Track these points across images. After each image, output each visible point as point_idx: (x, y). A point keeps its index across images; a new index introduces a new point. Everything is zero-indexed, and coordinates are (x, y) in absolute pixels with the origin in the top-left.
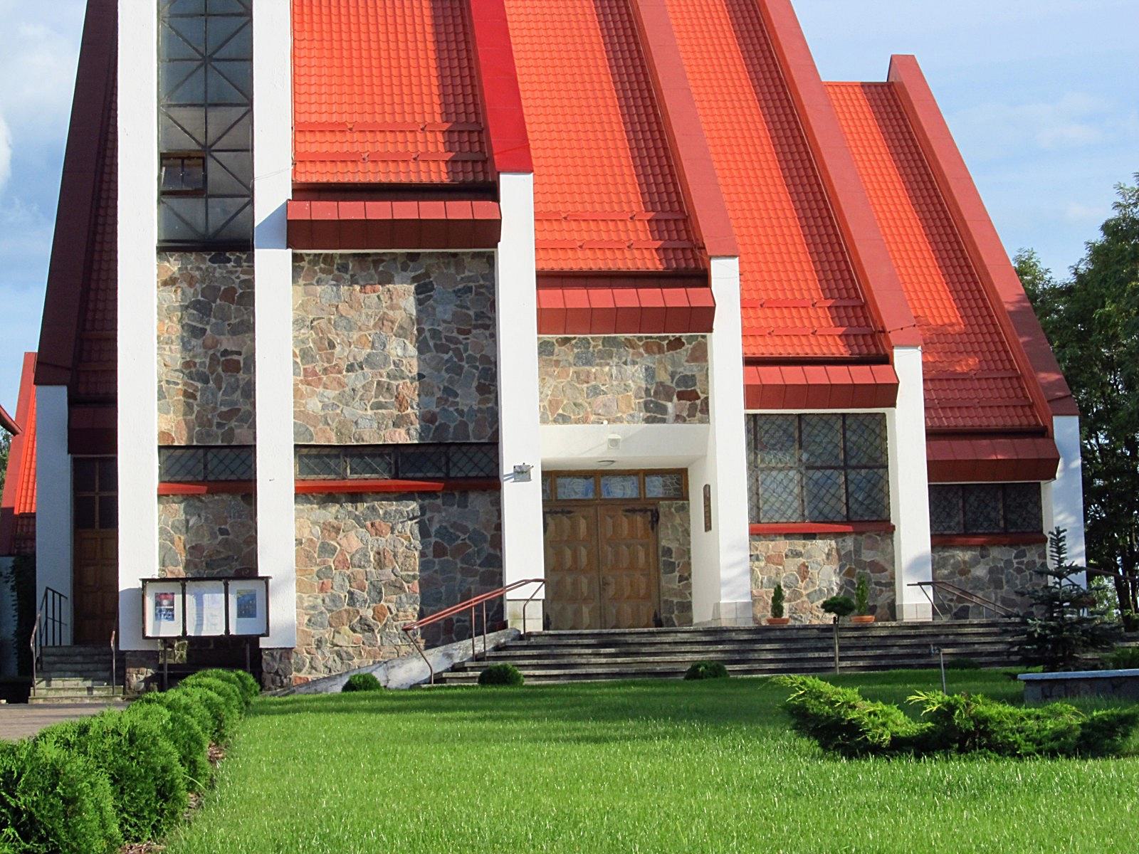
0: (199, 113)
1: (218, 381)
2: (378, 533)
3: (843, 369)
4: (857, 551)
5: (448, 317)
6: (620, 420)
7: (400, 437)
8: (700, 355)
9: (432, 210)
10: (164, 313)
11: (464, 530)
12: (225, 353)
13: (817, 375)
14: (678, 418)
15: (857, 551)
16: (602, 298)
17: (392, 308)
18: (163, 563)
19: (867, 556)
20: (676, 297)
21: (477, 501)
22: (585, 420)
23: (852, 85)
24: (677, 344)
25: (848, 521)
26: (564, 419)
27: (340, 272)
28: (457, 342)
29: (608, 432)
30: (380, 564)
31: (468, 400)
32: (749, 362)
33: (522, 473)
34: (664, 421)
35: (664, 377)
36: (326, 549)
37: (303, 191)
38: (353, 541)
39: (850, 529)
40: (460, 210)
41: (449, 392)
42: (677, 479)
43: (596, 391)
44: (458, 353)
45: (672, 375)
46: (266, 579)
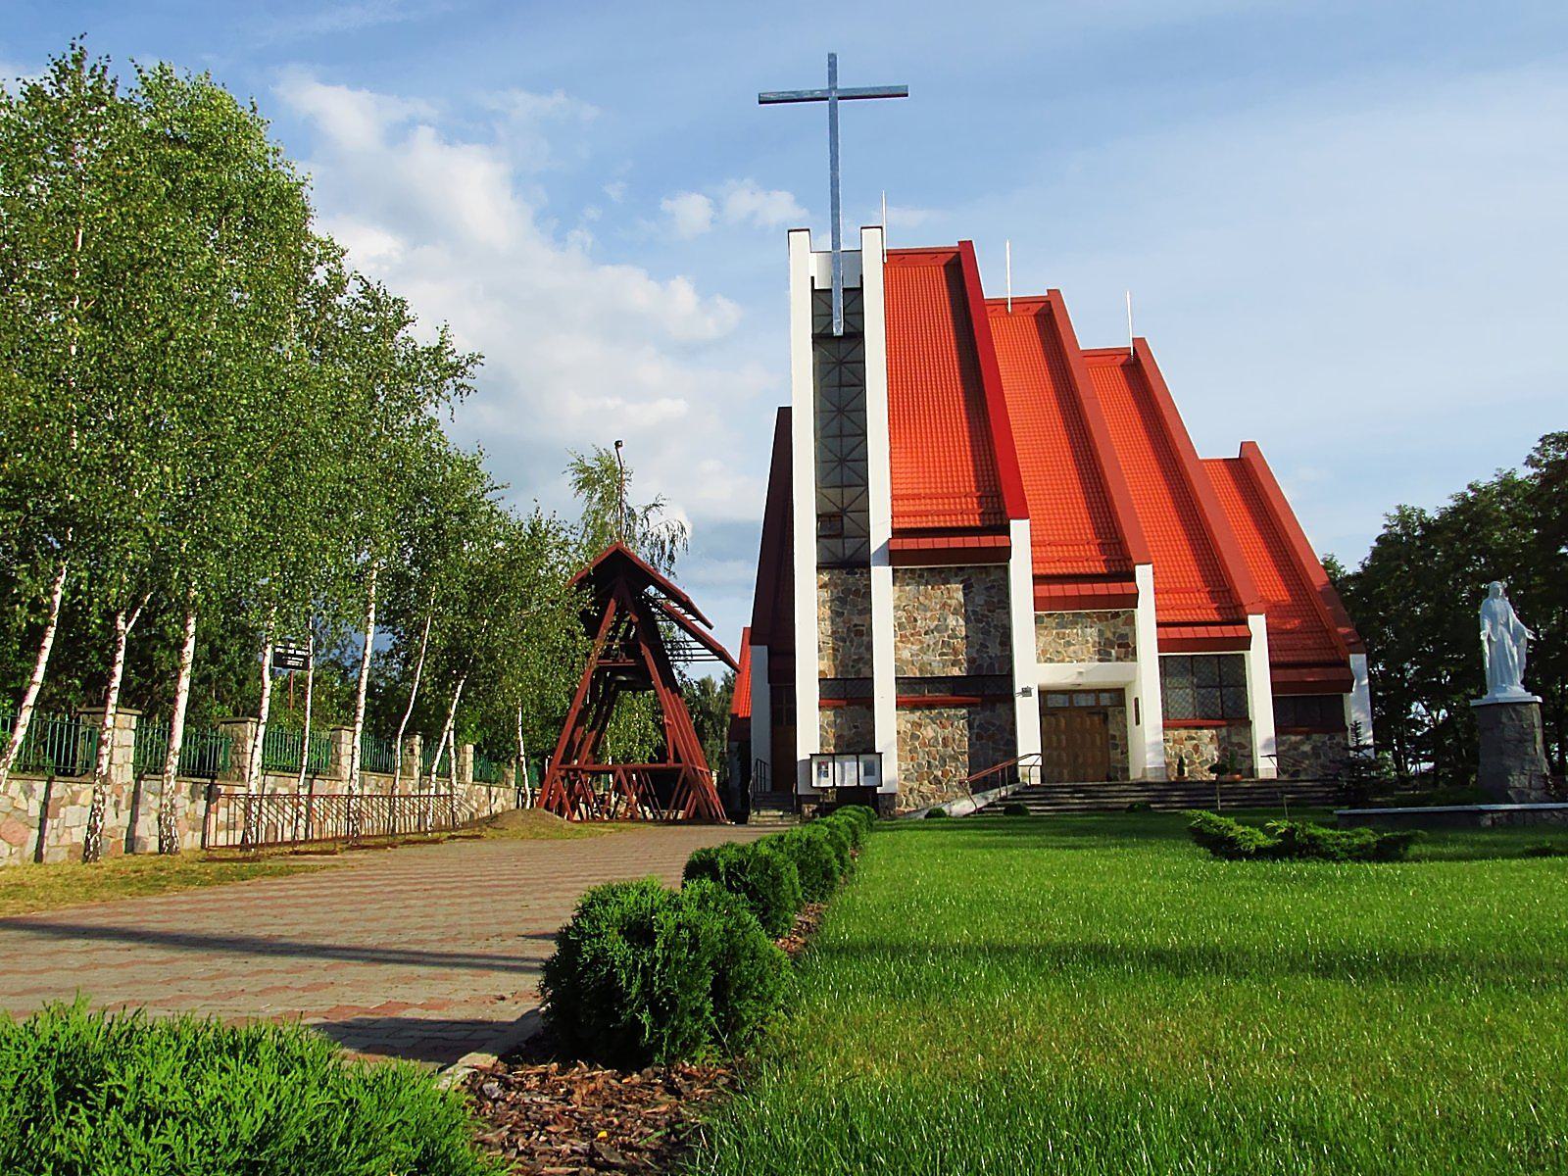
0: (839, 490)
1: (851, 642)
2: (944, 727)
3: (1217, 628)
4: (1229, 736)
5: (982, 602)
6: (1083, 660)
7: (956, 672)
8: (1131, 621)
9: (972, 542)
10: (821, 604)
11: (994, 725)
12: (855, 625)
13: (1201, 632)
14: (1118, 659)
15: (1229, 736)
16: (1071, 589)
17: (949, 598)
18: (822, 745)
19: (1235, 739)
20: (1115, 588)
21: (1001, 709)
22: (1063, 661)
23: (1218, 460)
24: (1116, 615)
25: (1223, 718)
26: (1051, 660)
27: (919, 578)
28: (987, 617)
29: (1082, 667)
30: (945, 745)
31: (994, 650)
32: (1159, 625)
33: (1026, 692)
34: (1109, 661)
35: (1109, 635)
36: (914, 737)
37: (897, 533)
38: (929, 732)
39: (1224, 723)
40: (987, 541)
41: (983, 646)
42: (1118, 695)
43: (1069, 644)
44: (988, 623)
45: (1114, 633)
46: (880, 754)
